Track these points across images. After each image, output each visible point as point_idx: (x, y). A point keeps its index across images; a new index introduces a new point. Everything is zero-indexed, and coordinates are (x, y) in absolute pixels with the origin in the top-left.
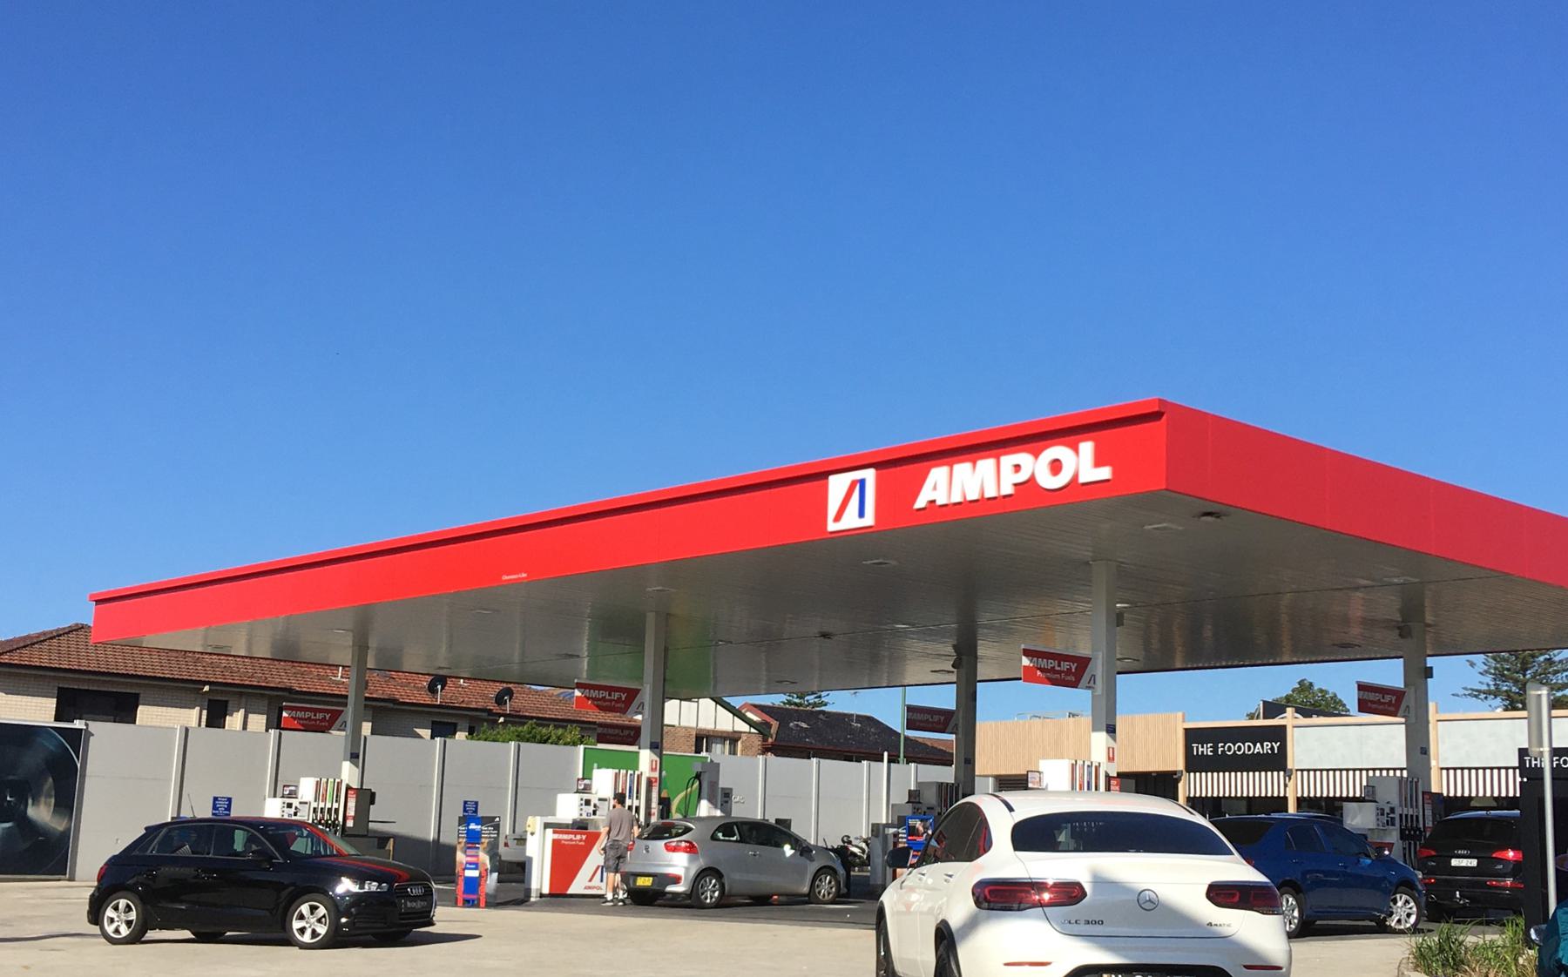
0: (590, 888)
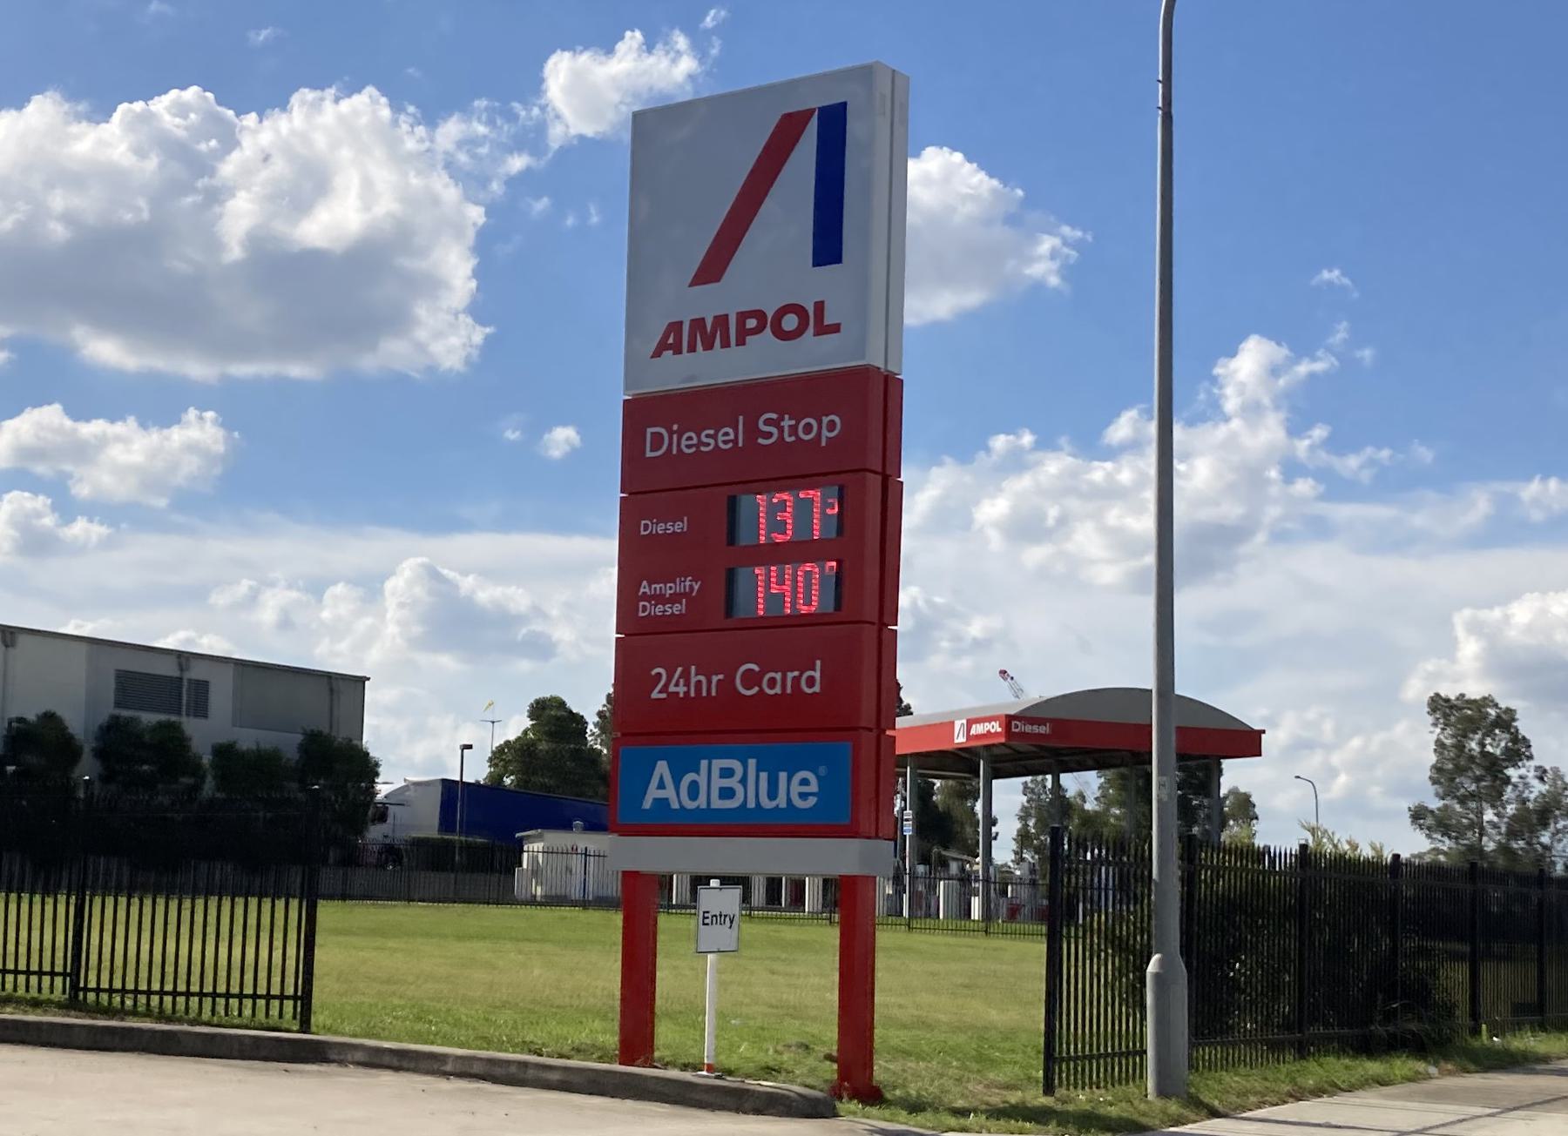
0: (709, 333)
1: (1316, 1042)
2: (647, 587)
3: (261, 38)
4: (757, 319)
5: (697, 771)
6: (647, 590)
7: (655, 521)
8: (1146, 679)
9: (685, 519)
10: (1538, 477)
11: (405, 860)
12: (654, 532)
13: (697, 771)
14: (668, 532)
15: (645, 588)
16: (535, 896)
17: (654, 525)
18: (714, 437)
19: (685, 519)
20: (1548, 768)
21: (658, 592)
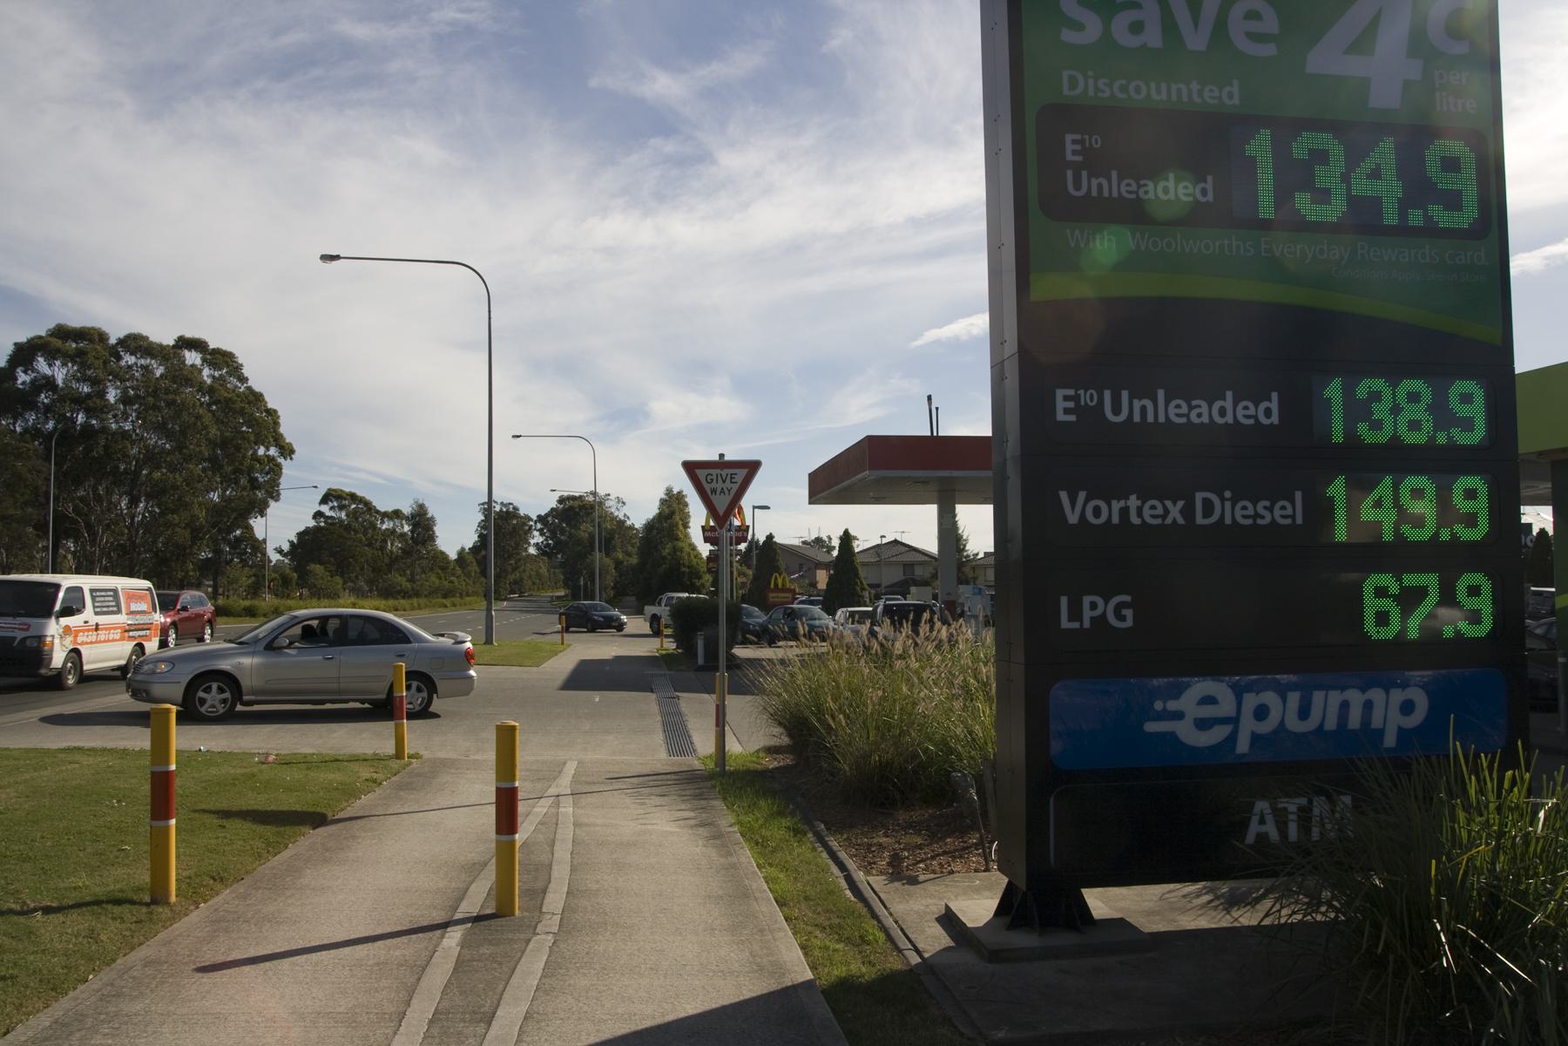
1: (62, 478)
2: (1269, 819)
3: (384, 527)
4: (1230, 490)
5: (1270, 400)
6: (1271, 829)
7: (1228, 494)
8: (929, 434)
9: (1298, 495)
10: (295, 541)
11: (931, 683)
12: (1228, 521)
13: (1270, 400)
14: (1260, 521)
15: (1262, 821)
16: (1380, 733)
17: (1228, 505)
18: (1270, 509)
19: (1298, 495)
20: (317, 508)
21: (1354, 721)
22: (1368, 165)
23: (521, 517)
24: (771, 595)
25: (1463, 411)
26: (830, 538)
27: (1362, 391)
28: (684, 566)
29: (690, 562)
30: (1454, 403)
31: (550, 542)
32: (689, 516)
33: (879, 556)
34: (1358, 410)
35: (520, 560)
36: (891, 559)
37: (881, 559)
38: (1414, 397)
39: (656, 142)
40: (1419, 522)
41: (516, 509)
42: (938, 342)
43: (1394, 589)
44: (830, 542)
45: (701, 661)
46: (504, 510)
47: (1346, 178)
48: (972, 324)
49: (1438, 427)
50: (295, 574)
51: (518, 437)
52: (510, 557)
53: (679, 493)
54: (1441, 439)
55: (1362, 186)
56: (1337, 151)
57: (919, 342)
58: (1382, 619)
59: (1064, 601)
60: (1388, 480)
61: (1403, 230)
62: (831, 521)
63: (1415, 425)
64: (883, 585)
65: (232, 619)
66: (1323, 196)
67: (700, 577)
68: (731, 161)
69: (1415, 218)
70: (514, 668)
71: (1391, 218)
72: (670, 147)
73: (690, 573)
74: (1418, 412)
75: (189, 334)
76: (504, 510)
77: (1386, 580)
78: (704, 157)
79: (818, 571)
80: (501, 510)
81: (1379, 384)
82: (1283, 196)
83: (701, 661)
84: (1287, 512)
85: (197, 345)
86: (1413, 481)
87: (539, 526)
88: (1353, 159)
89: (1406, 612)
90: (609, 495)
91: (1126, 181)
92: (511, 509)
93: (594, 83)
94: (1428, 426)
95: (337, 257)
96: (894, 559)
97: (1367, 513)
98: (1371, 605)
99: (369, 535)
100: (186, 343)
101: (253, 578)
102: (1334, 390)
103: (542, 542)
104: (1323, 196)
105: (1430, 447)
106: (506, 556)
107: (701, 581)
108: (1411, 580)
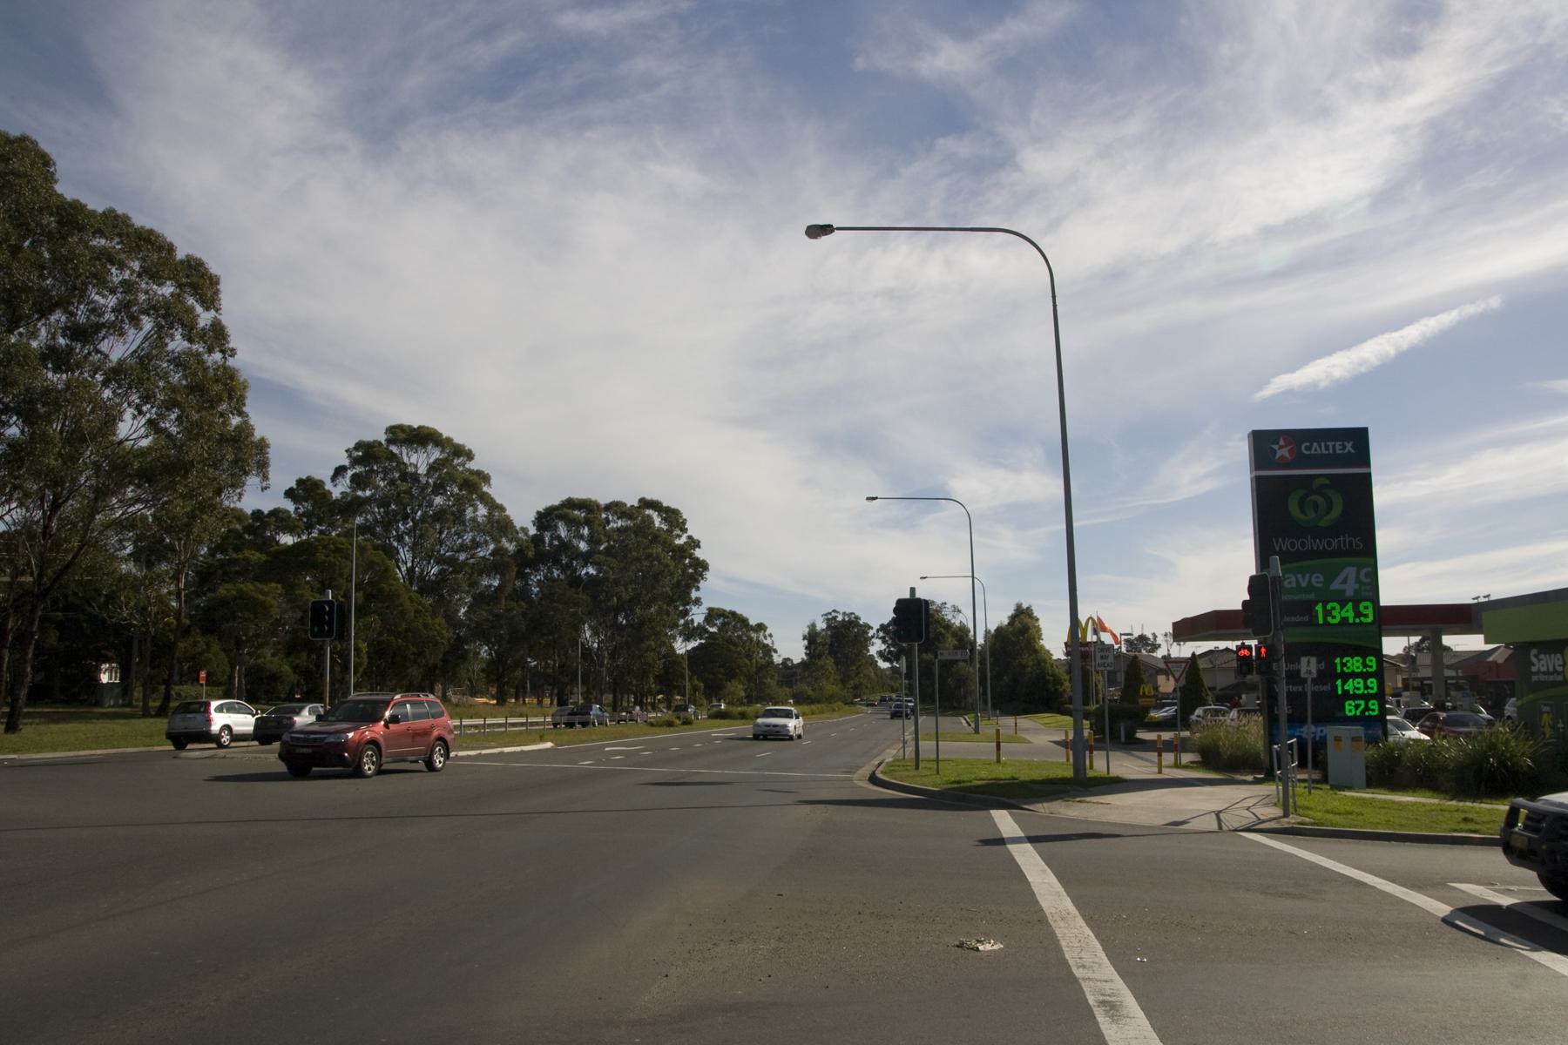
22: (1345, 610)
23: (861, 626)
24: (1140, 700)
25: (1370, 664)
26: (1155, 636)
27: (1344, 661)
28: (1048, 674)
29: (1053, 671)
30: (1368, 662)
31: (892, 649)
32: (78, 201)
33: (1212, 662)
34: (1343, 665)
35: (860, 666)
36: (1224, 666)
37: (1214, 667)
38: (1358, 661)
39: (947, 144)
40: (1359, 689)
41: (857, 618)
42: (1290, 392)
43: (1353, 704)
44: (1155, 639)
45: (1123, 739)
46: (847, 619)
47: (1340, 613)
48: (1334, 366)
49: (1364, 667)
50: (702, 684)
51: (925, 578)
52: (853, 663)
53: (1028, 608)
54: (1365, 670)
55: (1344, 614)
56: (1338, 607)
57: (1267, 392)
58: (1350, 711)
59: (607, 749)
60: (1351, 680)
61: (1354, 624)
62: (1187, 650)
63: (1358, 668)
64: (1218, 688)
65: (731, 721)
66: (1334, 617)
67: (1062, 684)
68: (1039, 163)
69: (1357, 621)
70: (1013, 744)
71: (1351, 621)
72: (962, 147)
73: (1054, 680)
74: (1359, 664)
75: (649, 497)
76: (847, 619)
77: (1351, 702)
78: (1001, 160)
79: (1159, 677)
80: (844, 620)
81: (1349, 658)
82: (1325, 617)
83: (1123, 739)
84: (1327, 688)
85: (654, 505)
86: (1357, 680)
87: (881, 634)
88: (1342, 608)
89: (1356, 709)
90: (945, 603)
91: (1316, 575)
92: (853, 619)
93: (860, 63)
94: (1361, 667)
95: (877, 498)
96: (1227, 665)
97: (1346, 687)
98: (1347, 708)
99: (747, 648)
100: (646, 504)
101: (1542, 724)
102: (1338, 661)
103: (885, 650)
104: (1334, 617)
105: (1362, 673)
106: (849, 663)
107: (1063, 687)
108: (1358, 702)
